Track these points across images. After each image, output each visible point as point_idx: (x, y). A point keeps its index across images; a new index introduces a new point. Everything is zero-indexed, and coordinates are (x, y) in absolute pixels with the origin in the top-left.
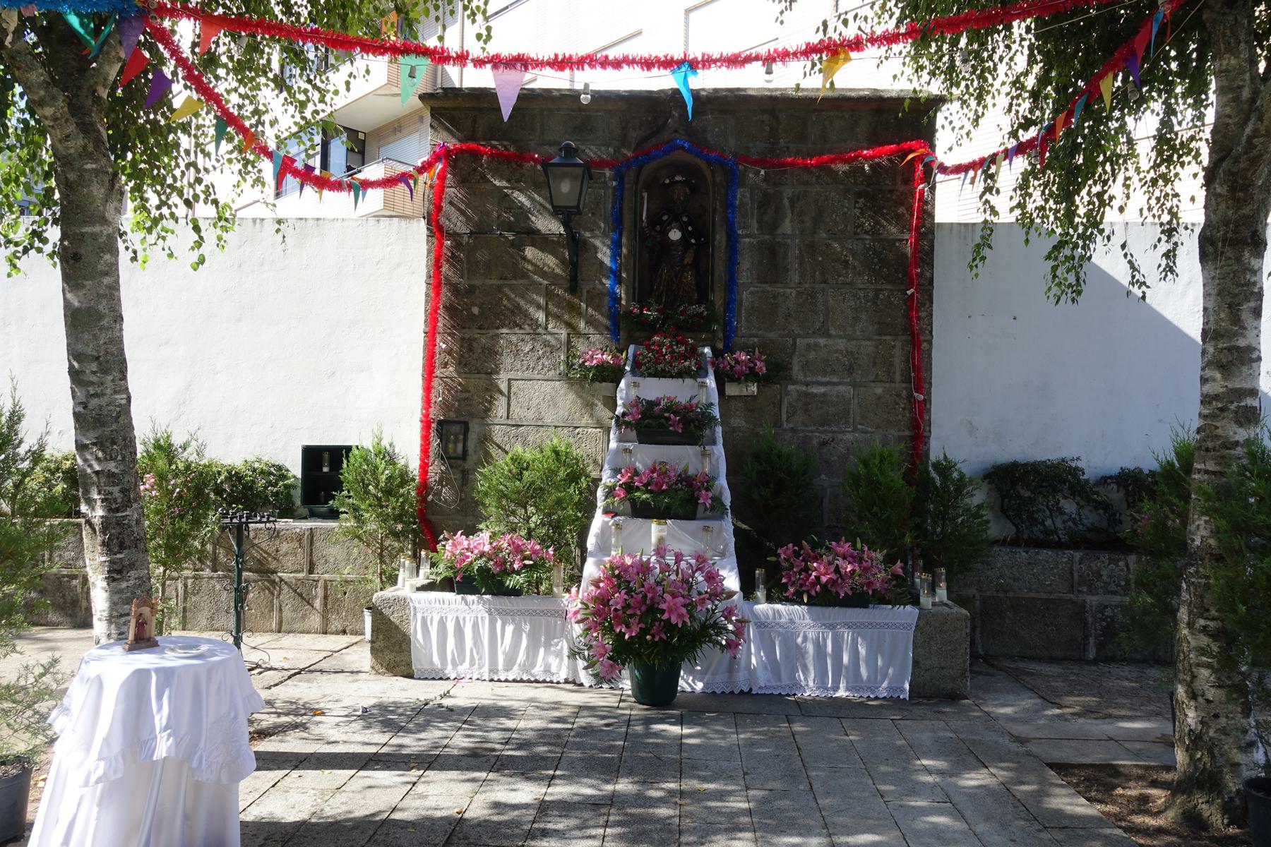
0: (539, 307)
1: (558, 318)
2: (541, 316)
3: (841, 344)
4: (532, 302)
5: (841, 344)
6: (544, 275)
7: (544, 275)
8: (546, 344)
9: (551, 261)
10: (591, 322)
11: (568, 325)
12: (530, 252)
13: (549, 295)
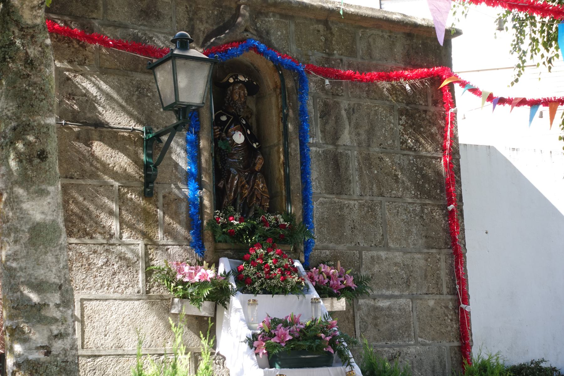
0: (111, 213)
1: (132, 227)
3: (398, 257)
5: (398, 257)
6: (115, 175)
7: (115, 175)
8: (121, 257)
9: (120, 161)
10: (168, 232)
11: (145, 235)
13: (121, 200)
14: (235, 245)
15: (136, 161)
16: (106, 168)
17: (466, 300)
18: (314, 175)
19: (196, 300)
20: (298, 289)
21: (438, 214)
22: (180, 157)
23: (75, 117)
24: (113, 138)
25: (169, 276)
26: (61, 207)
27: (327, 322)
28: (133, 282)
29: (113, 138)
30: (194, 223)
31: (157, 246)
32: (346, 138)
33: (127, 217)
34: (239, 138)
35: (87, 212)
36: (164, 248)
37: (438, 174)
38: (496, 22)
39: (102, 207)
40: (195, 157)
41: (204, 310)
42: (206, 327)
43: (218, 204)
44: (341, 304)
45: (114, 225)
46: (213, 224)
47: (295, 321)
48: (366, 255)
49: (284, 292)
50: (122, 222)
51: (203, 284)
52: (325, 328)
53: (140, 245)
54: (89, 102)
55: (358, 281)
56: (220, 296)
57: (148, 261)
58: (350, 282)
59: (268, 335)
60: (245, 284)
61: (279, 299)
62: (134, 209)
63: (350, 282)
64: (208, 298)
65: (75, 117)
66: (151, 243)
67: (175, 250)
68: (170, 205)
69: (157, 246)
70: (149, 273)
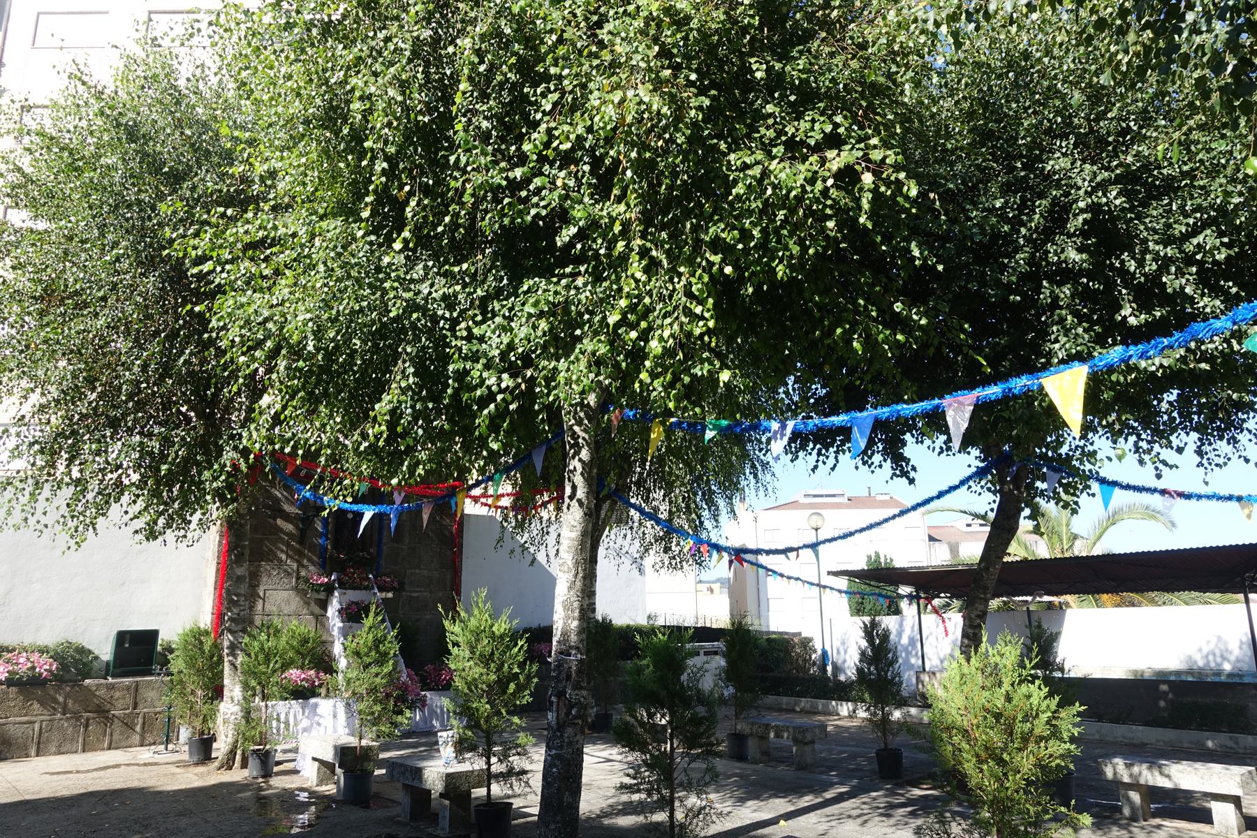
0: (282, 551)
1: (292, 558)
2: (284, 557)
3: (425, 573)
4: (279, 549)
5: (425, 573)
6: (286, 534)
7: (286, 534)
8: (285, 571)
9: (289, 527)
10: (310, 560)
11: (298, 561)
12: (279, 522)
13: (288, 545)
14: (340, 567)
15: (297, 527)
16: (281, 530)
19: (318, 591)
21: (449, 553)
23: (269, 507)
24: (287, 517)
25: (307, 581)
26: (576, 614)
27: (142, 484)
28: (290, 582)
29: (287, 517)
31: (303, 566)
33: (290, 553)
35: (803, 730)
36: (306, 567)
37: (451, 533)
39: (279, 549)
41: (322, 596)
42: (324, 605)
43: (335, 547)
44: (390, 595)
45: (284, 557)
46: (331, 556)
48: (408, 572)
50: (288, 556)
51: (321, 585)
53: (295, 566)
54: (277, 500)
56: (329, 589)
57: (298, 572)
58: (396, 584)
59: (349, 607)
60: (343, 585)
62: (293, 549)
63: (396, 584)
65: (269, 507)
66: (300, 565)
67: (311, 568)
68: (312, 548)
69: (303, 566)
70: (298, 578)
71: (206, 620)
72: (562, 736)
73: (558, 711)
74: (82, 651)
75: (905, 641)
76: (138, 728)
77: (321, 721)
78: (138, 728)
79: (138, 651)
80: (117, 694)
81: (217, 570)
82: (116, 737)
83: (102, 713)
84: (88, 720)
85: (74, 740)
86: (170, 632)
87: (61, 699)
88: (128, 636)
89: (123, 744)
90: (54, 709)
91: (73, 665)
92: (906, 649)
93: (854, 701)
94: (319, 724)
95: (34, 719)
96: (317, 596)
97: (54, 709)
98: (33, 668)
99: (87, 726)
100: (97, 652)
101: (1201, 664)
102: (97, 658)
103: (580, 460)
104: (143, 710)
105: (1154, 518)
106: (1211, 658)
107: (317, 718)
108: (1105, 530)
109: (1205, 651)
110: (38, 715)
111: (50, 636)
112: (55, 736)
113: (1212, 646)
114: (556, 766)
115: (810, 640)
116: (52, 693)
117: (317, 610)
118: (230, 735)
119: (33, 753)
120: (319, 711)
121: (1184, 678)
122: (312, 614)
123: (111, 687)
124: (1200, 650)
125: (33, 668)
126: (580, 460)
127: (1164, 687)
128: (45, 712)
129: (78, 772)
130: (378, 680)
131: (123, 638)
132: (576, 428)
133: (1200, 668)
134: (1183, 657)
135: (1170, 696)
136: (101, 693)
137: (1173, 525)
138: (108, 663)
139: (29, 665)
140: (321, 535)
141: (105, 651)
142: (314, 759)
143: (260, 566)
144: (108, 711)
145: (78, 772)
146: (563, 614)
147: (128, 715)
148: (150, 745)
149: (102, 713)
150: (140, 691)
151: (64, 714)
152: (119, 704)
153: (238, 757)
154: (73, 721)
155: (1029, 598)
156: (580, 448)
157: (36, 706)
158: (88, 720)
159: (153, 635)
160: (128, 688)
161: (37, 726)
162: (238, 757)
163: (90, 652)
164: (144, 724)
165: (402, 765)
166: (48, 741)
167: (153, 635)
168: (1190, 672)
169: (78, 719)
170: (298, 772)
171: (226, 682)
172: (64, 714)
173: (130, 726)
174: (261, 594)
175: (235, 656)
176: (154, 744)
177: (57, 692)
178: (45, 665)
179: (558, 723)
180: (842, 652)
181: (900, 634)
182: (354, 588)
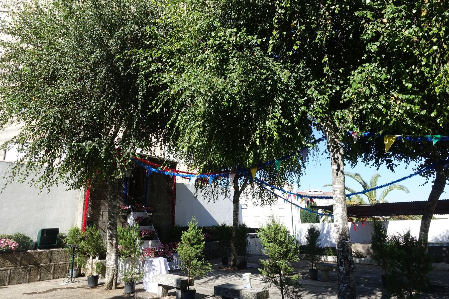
10: (120, 200)
17: (174, 214)
18: (148, 189)
19: (125, 213)
20: (144, 211)
22: (123, 186)
30: (125, 198)
32: (155, 182)
34: (134, 182)
35: (105, 195)
37: (171, 189)
38: (398, 234)
40: (126, 186)
43: (129, 194)
44: (151, 214)
46: (128, 198)
47: (143, 217)
49: (141, 212)
51: (126, 210)
52: (148, 218)
55: (154, 210)
56: (129, 212)
60: (134, 210)
61: (140, 213)
64: (340, 129)
67: (121, 203)
68: (121, 194)
71: (79, 225)
72: (349, 277)
73: (345, 266)
74: (25, 237)
75: (325, 232)
76: (52, 271)
77: (155, 268)
78: (52, 271)
79: (50, 238)
80: (43, 257)
81: (84, 203)
82: (42, 275)
83: (37, 265)
84: (31, 268)
85: (25, 277)
86: (65, 230)
87: (19, 259)
88: (46, 231)
89: (45, 278)
90: (16, 263)
91: (23, 243)
92: (325, 235)
93: (326, 255)
94: (154, 269)
95: (7, 268)
96: (123, 214)
97: (16, 263)
98: (8, 246)
99: (30, 271)
100: (31, 238)
101: (441, 240)
102: (32, 241)
103: (340, 154)
104: (54, 263)
105: (402, 189)
106: (444, 238)
107: (153, 267)
108: (387, 193)
109: (442, 235)
110: (9, 267)
111: (11, 231)
112: (17, 276)
113: (445, 233)
114: (348, 292)
115: (289, 232)
116: (15, 256)
117: (123, 220)
118: (110, 275)
119: (7, 283)
120: (153, 263)
121: (435, 245)
122: (121, 222)
123: (40, 254)
124: (440, 235)
125: (8, 246)
126: (340, 154)
127: (444, 249)
128: (12, 265)
129: (39, 293)
130: (199, 251)
131: (44, 232)
132: (336, 140)
133: (440, 242)
134: (434, 238)
135: (447, 252)
136: (37, 256)
137: (408, 192)
138: (36, 243)
139: (6, 244)
140: (124, 189)
141: (35, 238)
142: (159, 285)
143: (101, 202)
144: (39, 264)
145: (39, 293)
146: (342, 222)
147: (48, 266)
148: (57, 278)
149: (37, 265)
150: (53, 255)
151: (20, 266)
152: (44, 261)
153: (114, 284)
154: (24, 269)
155: (380, 217)
156: (339, 149)
157: (8, 262)
158: (31, 268)
159: (57, 230)
160: (48, 254)
161: (9, 272)
162: (114, 284)
163: (29, 238)
164: (54, 269)
165: (225, 289)
166: (14, 278)
167: (57, 230)
168: (437, 243)
169: (26, 268)
170: (145, 290)
171: (108, 251)
172: (20, 266)
173: (48, 271)
174: (101, 213)
175: (112, 240)
176: (58, 278)
177: (18, 256)
178: (13, 245)
179: (346, 272)
180: (300, 236)
181: (323, 229)
182: (139, 211)
